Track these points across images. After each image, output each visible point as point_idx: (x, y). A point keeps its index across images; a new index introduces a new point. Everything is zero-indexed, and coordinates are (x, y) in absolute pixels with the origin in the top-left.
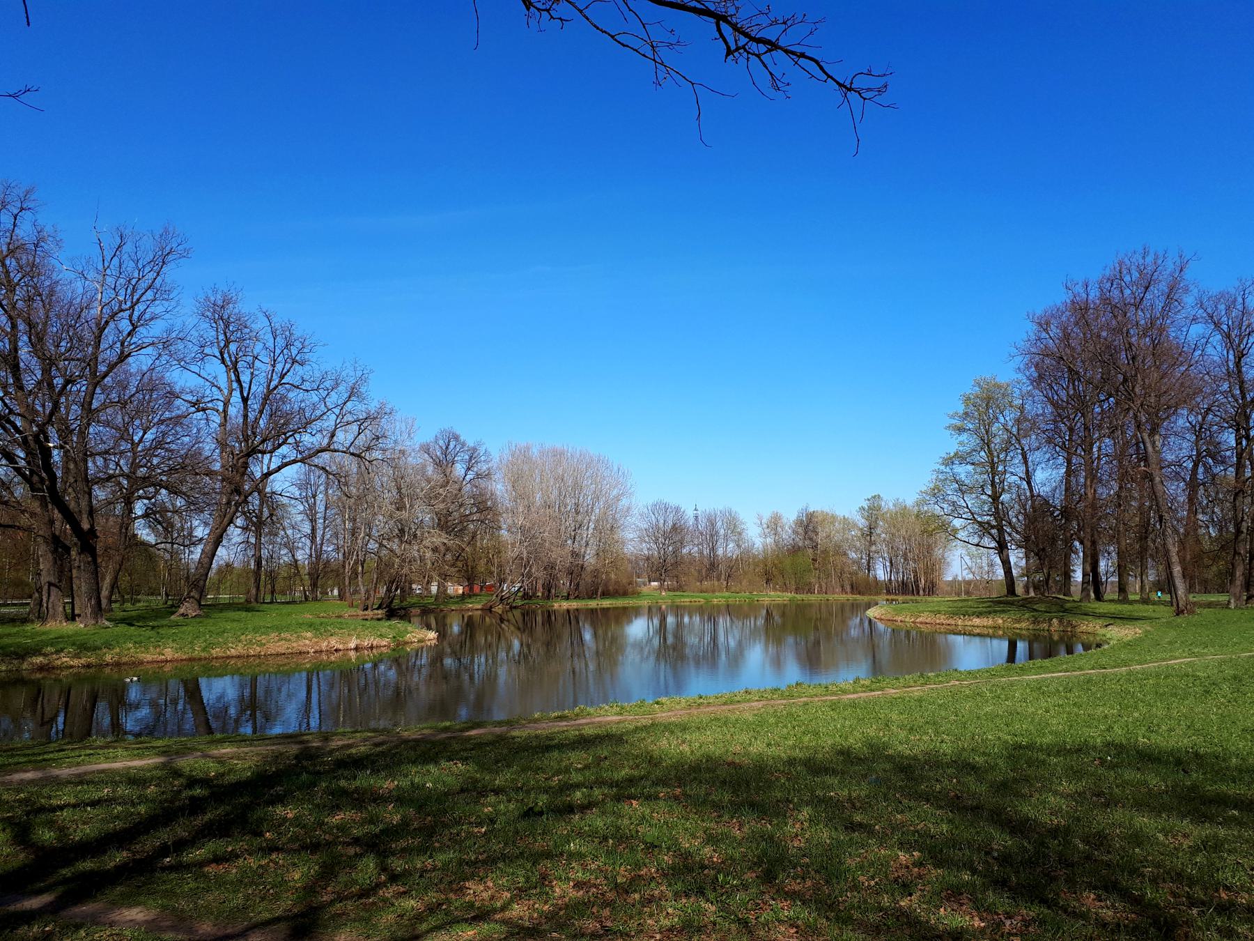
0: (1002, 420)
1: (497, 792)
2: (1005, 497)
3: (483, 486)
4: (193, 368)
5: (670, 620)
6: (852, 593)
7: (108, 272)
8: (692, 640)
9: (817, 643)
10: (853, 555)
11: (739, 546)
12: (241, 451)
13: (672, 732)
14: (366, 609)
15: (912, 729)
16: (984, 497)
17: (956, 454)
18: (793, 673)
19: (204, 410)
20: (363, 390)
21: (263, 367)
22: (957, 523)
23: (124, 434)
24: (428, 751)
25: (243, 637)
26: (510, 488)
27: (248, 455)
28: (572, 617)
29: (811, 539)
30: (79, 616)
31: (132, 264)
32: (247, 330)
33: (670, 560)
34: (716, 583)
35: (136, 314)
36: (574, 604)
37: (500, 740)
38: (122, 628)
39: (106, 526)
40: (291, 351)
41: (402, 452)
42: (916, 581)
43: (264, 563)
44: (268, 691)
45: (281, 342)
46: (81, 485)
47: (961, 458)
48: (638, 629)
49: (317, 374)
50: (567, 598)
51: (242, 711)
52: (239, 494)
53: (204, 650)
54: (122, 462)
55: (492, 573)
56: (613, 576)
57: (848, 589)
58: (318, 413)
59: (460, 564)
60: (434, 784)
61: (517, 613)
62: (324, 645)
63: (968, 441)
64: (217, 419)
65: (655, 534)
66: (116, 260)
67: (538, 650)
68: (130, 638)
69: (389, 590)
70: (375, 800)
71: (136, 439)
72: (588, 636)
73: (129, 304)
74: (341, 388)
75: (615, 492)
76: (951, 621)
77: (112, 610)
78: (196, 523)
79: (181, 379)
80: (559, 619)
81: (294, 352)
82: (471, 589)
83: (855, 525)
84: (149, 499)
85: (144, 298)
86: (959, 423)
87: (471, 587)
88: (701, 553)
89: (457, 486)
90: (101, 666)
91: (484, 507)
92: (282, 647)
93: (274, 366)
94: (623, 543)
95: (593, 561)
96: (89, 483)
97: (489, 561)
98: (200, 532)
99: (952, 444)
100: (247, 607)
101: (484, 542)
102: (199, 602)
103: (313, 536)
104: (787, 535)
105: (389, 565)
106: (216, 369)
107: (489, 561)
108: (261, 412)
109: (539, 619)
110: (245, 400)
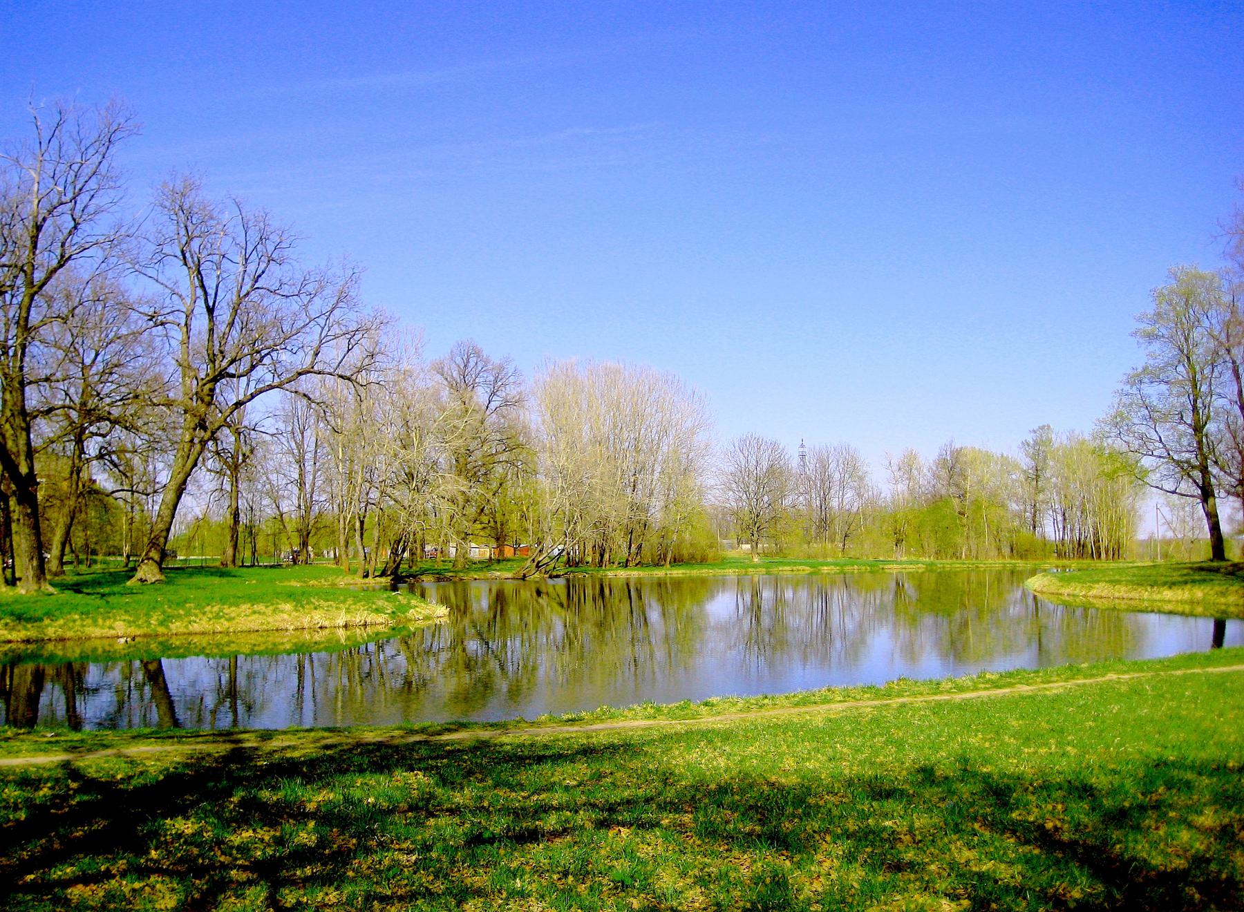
0: (1207, 323)
1: (452, 812)
2: (1211, 427)
3: (513, 415)
4: (150, 272)
5: (767, 594)
6: (1012, 557)
7: (46, 156)
8: (794, 621)
9: (964, 625)
10: (1014, 506)
11: (860, 495)
12: (207, 375)
13: (710, 742)
14: (366, 576)
15: (1028, 739)
16: (1182, 427)
17: (1145, 369)
18: (930, 663)
19: (162, 324)
20: (352, 294)
21: (234, 269)
22: (1147, 462)
23: (72, 354)
24: (383, 758)
25: (208, 609)
26: (548, 418)
27: (215, 380)
28: (632, 592)
29: (957, 486)
30: (20, 579)
31: (74, 146)
32: (213, 223)
33: (766, 515)
34: (829, 546)
35: (79, 207)
36: (634, 574)
37: (481, 747)
38: (68, 595)
39: (50, 472)
40: (265, 249)
41: (408, 374)
42: (1097, 541)
43: (242, 515)
44: (250, 676)
45: (254, 236)
46: (19, 421)
47: (1150, 375)
48: (722, 606)
49: (299, 276)
50: (626, 565)
51: (220, 702)
52: (205, 429)
53: (162, 623)
54: (72, 390)
55: (526, 531)
56: (687, 536)
57: (1006, 551)
58: (300, 324)
59: (485, 519)
60: (377, 799)
61: (561, 582)
62: (306, 621)
63: (1162, 352)
64: (178, 334)
65: (741, 478)
66: (55, 142)
67: (587, 630)
68: (75, 608)
69: (395, 553)
70: (294, 817)
71: (88, 361)
72: (654, 615)
73: (70, 195)
74: (328, 291)
75: (689, 424)
76: (1133, 594)
77: (63, 572)
78: (160, 466)
79: (138, 288)
80: (615, 591)
81: (271, 248)
82: (501, 552)
83: (1017, 466)
84: (104, 436)
85: (87, 188)
86: (1149, 328)
87: (500, 547)
88: (809, 504)
89: (479, 417)
90: (40, 641)
91: (513, 444)
92: (254, 622)
93: (245, 265)
94: (700, 493)
95: (659, 515)
96: (25, 417)
97: (524, 517)
98: (164, 477)
99: (1139, 356)
100: (221, 572)
101: (515, 490)
102: (159, 564)
103: (301, 484)
104: (925, 478)
105: (393, 519)
106: (181, 275)
107: (524, 517)
108: (232, 324)
109: (589, 592)
110: (210, 311)
